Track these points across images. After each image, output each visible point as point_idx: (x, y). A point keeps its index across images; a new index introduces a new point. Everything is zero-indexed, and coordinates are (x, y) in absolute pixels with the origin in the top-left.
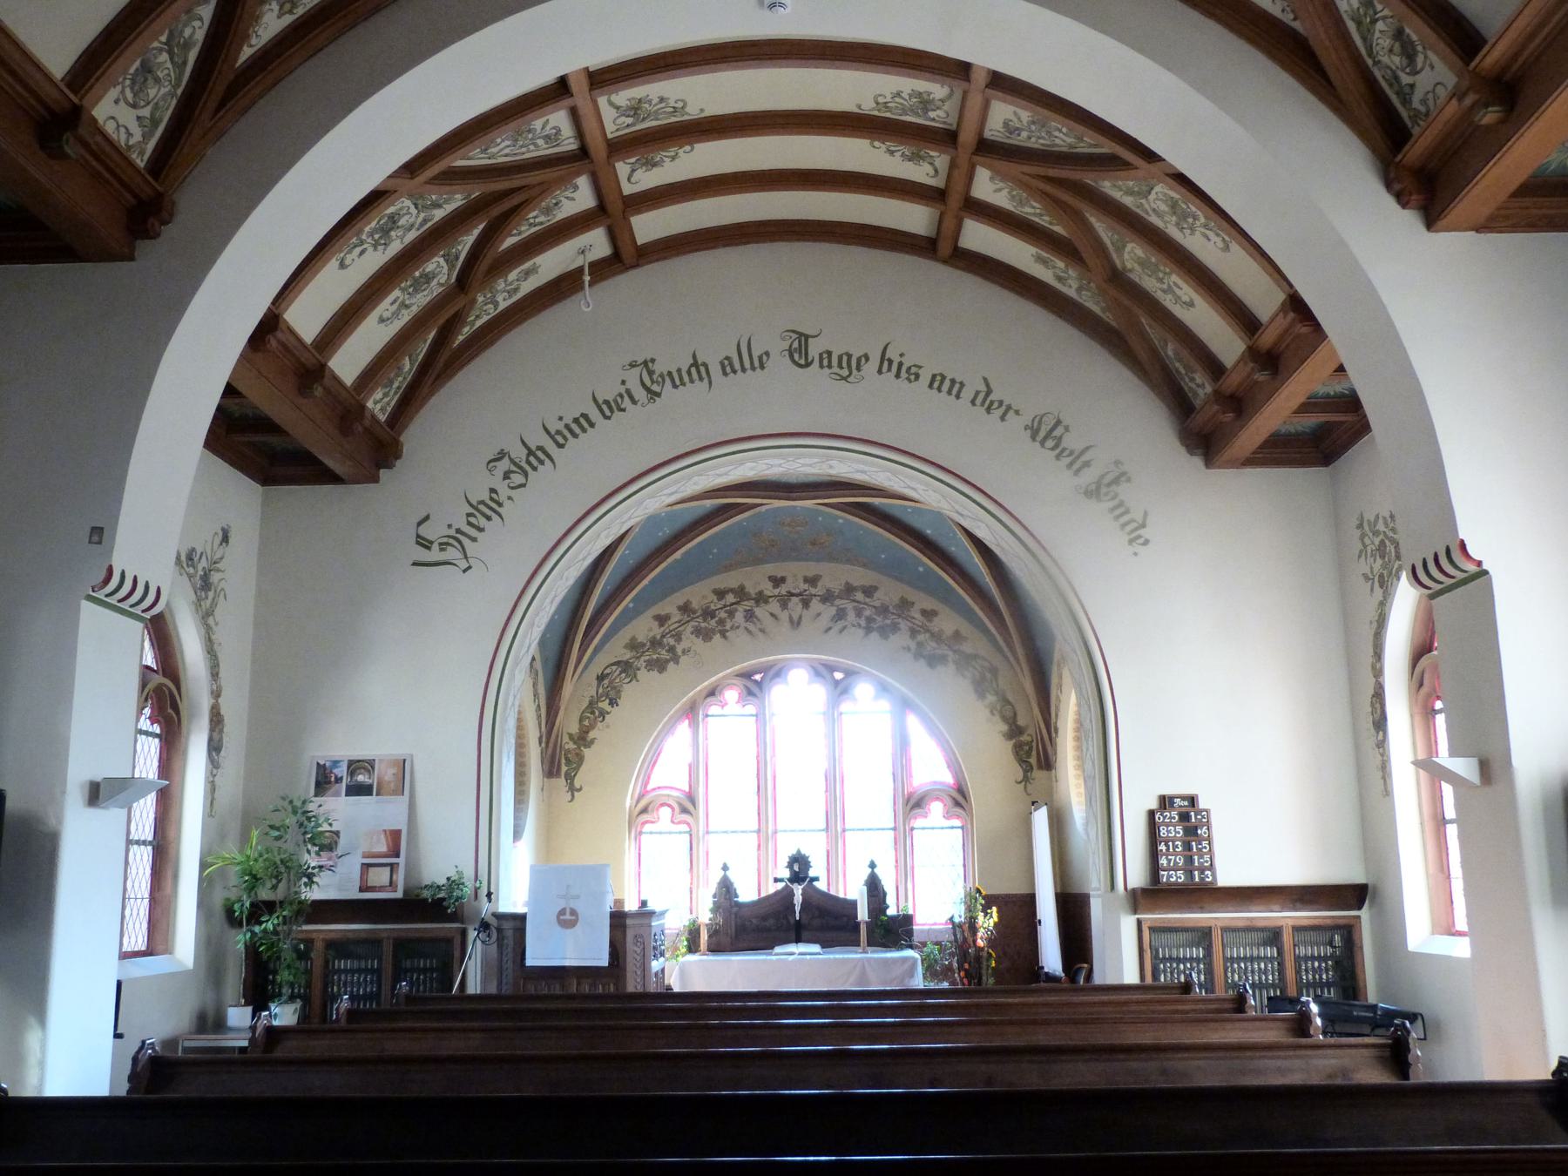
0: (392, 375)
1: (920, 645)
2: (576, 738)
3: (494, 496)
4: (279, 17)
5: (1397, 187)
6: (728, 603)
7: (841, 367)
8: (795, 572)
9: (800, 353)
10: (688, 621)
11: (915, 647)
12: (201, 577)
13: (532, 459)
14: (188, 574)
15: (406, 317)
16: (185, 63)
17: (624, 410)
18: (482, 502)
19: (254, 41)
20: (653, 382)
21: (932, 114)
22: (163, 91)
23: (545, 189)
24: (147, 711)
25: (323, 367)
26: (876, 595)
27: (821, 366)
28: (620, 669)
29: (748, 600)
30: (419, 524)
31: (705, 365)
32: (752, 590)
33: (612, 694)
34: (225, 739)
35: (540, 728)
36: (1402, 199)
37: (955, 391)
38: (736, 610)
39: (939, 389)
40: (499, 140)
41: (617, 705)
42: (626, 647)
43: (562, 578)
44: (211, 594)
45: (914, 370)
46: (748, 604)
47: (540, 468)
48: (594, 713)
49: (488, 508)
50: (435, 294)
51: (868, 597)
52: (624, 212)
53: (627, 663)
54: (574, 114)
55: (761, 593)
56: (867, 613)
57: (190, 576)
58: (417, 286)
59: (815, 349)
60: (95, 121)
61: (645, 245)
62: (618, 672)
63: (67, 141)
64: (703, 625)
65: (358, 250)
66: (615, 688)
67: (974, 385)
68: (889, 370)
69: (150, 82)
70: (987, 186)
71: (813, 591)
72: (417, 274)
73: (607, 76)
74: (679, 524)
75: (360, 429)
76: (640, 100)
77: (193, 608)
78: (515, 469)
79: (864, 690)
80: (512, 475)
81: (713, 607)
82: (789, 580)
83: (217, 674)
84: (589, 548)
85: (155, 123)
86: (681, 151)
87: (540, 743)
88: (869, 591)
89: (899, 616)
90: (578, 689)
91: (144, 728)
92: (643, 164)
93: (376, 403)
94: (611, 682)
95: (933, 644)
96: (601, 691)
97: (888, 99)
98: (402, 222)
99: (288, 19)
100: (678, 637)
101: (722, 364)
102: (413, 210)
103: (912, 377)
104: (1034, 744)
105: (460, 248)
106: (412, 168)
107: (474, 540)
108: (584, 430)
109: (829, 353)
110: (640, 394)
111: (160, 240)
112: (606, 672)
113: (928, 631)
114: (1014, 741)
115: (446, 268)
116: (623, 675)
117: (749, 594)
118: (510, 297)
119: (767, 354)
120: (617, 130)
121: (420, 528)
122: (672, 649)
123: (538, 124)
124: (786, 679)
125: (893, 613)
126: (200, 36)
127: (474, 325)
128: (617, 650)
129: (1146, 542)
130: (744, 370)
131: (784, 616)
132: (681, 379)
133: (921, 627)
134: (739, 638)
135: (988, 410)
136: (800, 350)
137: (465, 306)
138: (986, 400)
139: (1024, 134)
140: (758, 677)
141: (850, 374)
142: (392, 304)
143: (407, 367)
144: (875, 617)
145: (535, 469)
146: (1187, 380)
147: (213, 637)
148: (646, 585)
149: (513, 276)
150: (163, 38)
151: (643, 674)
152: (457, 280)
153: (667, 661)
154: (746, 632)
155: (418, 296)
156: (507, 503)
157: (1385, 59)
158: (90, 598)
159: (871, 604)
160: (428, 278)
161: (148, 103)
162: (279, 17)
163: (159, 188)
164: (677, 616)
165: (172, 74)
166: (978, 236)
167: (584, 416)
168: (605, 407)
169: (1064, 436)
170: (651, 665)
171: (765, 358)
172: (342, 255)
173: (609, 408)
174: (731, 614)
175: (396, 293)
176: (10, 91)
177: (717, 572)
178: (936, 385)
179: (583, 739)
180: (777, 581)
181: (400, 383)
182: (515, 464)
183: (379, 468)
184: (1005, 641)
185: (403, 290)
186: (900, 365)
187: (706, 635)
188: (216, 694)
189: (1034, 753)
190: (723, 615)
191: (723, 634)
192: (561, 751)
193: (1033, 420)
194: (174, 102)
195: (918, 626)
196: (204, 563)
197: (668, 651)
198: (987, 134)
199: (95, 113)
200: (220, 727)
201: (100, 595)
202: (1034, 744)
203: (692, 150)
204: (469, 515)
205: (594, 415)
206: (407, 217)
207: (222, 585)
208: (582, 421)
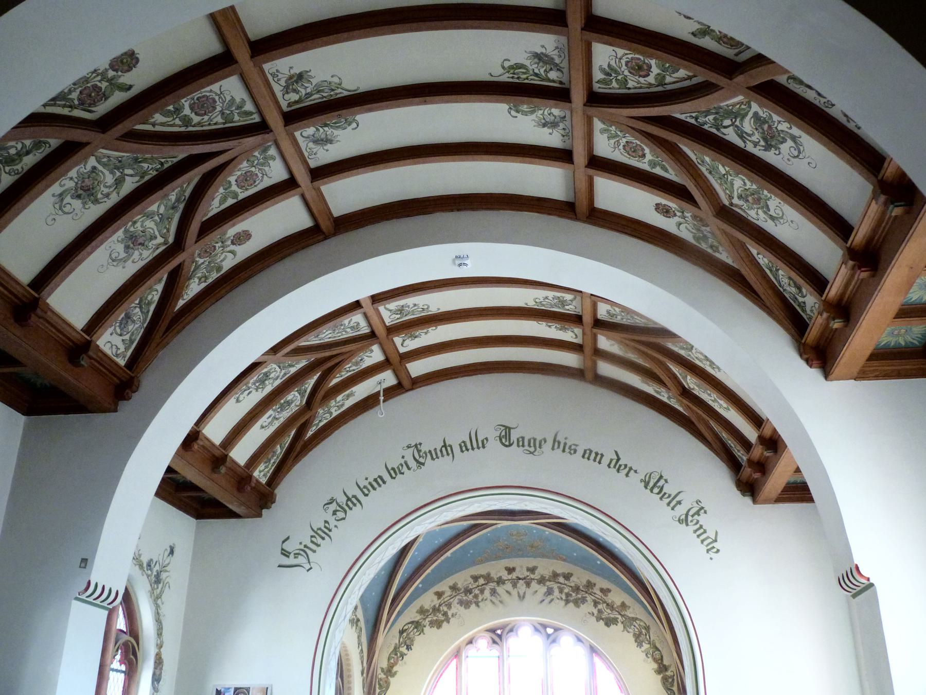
0: (270, 456)
1: (600, 611)
2: (385, 671)
3: (327, 525)
4: (198, 285)
5: (806, 356)
6: (480, 584)
7: (529, 446)
8: (521, 564)
9: (506, 439)
10: (456, 596)
11: (597, 612)
12: (155, 576)
13: (349, 503)
14: (147, 575)
15: (277, 424)
16: (148, 312)
17: (403, 473)
18: (320, 529)
19: (185, 297)
20: (420, 457)
21: (567, 307)
22: (137, 326)
23: (352, 354)
24: (118, 657)
25: (226, 456)
26: (571, 579)
27: (518, 446)
28: (413, 626)
29: (492, 582)
30: (284, 542)
31: (451, 446)
32: (494, 576)
33: (408, 642)
34: (163, 674)
35: (362, 663)
36: (808, 362)
37: (598, 459)
38: (484, 589)
39: (588, 459)
40: (325, 331)
41: (411, 649)
42: (417, 612)
43: (365, 574)
44: (160, 586)
45: (573, 447)
46: (492, 585)
47: (354, 508)
48: (397, 655)
49: (323, 532)
50: (294, 411)
51: (567, 580)
52: (400, 362)
53: (417, 622)
54: (365, 315)
55: (500, 577)
56: (566, 590)
57: (148, 576)
58: (282, 408)
59: (514, 436)
60: (98, 346)
61: (417, 378)
62: (412, 628)
63: (83, 358)
64: (464, 598)
65: (248, 391)
66: (410, 638)
67: (609, 455)
68: (559, 447)
69: (130, 322)
70: (605, 342)
71: (532, 576)
72: (282, 401)
73: (379, 297)
74: (448, 536)
75: (249, 488)
76: (403, 306)
77: (149, 594)
78: (340, 509)
79: (566, 640)
80: (338, 513)
81: (471, 587)
82: (517, 570)
83: (161, 634)
84: (381, 556)
85: (132, 341)
86: (430, 329)
87: (362, 674)
88: (567, 577)
89: (586, 592)
90: (387, 639)
91: (115, 668)
92: (409, 337)
93: (260, 472)
94: (408, 634)
95: (609, 611)
96: (401, 640)
97: (542, 300)
98: (272, 375)
99: (203, 285)
100: (449, 606)
101: (460, 445)
102: (278, 369)
103: (572, 452)
104: (675, 677)
105: (307, 386)
106: (275, 350)
107: (314, 551)
108: (380, 486)
109: (523, 438)
110: (412, 464)
111: (130, 401)
112: (405, 628)
113: (605, 602)
114: (662, 675)
115: (299, 397)
116: (415, 630)
117: (492, 578)
118: (339, 409)
119: (487, 439)
120: (392, 321)
121: (284, 544)
122: (445, 614)
123: (346, 322)
124: (517, 634)
125: (582, 591)
126: (156, 298)
127: (318, 425)
128: (411, 614)
129: (718, 551)
130: (473, 449)
131: (514, 592)
132: (436, 454)
133: (601, 600)
134: (486, 606)
135: (618, 471)
136: (505, 437)
137: (310, 418)
138: (617, 464)
139: (619, 317)
140: (499, 632)
141: (535, 451)
142: (268, 418)
143: (279, 451)
144: (571, 593)
145: (351, 509)
146: (736, 451)
147: (160, 612)
148: (429, 574)
149: (339, 398)
150: (137, 302)
151: (427, 629)
152: (306, 403)
153: (442, 621)
154: (491, 603)
155: (283, 413)
156: (334, 529)
157: (788, 289)
158: (77, 599)
159: (569, 584)
160: (289, 403)
161: (128, 333)
162: (198, 285)
163: (132, 374)
164: (448, 592)
165: (142, 318)
166: (606, 369)
167: (380, 477)
168: (392, 472)
169: (665, 486)
170: (432, 624)
171: (485, 441)
172: (237, 396)
173: (394, 472)
174: (482, 592)
175: (270, 412)
176: (54, 336)
177: (474, 563)
178: (587, 456)
179: (390, 672)
180: (510, 570)
181: (275, 460)
182: (340, 506)
183: (262, 509)
184: (653, 609)
185: (274, 410)
186: (565, 444)
187: (466, 604)
188: (160, 646)
189: (675, 683)
190: (477, 592)
191: (477, 605)
192: (376, 680)
193: (646, 476)
194: (143, 330)
195: (598, 599)
196: (157, 568)
197: (443, 615)
198: (599, 317)
199: (98, 343)
200: (161, 666)
201: (83, 597)
202: (675, 677)
203: (436, 329)
204: (312, 537)
205: (386, 477)
206: (274, 373)
207: (168, 580)
208: (379, 480)
